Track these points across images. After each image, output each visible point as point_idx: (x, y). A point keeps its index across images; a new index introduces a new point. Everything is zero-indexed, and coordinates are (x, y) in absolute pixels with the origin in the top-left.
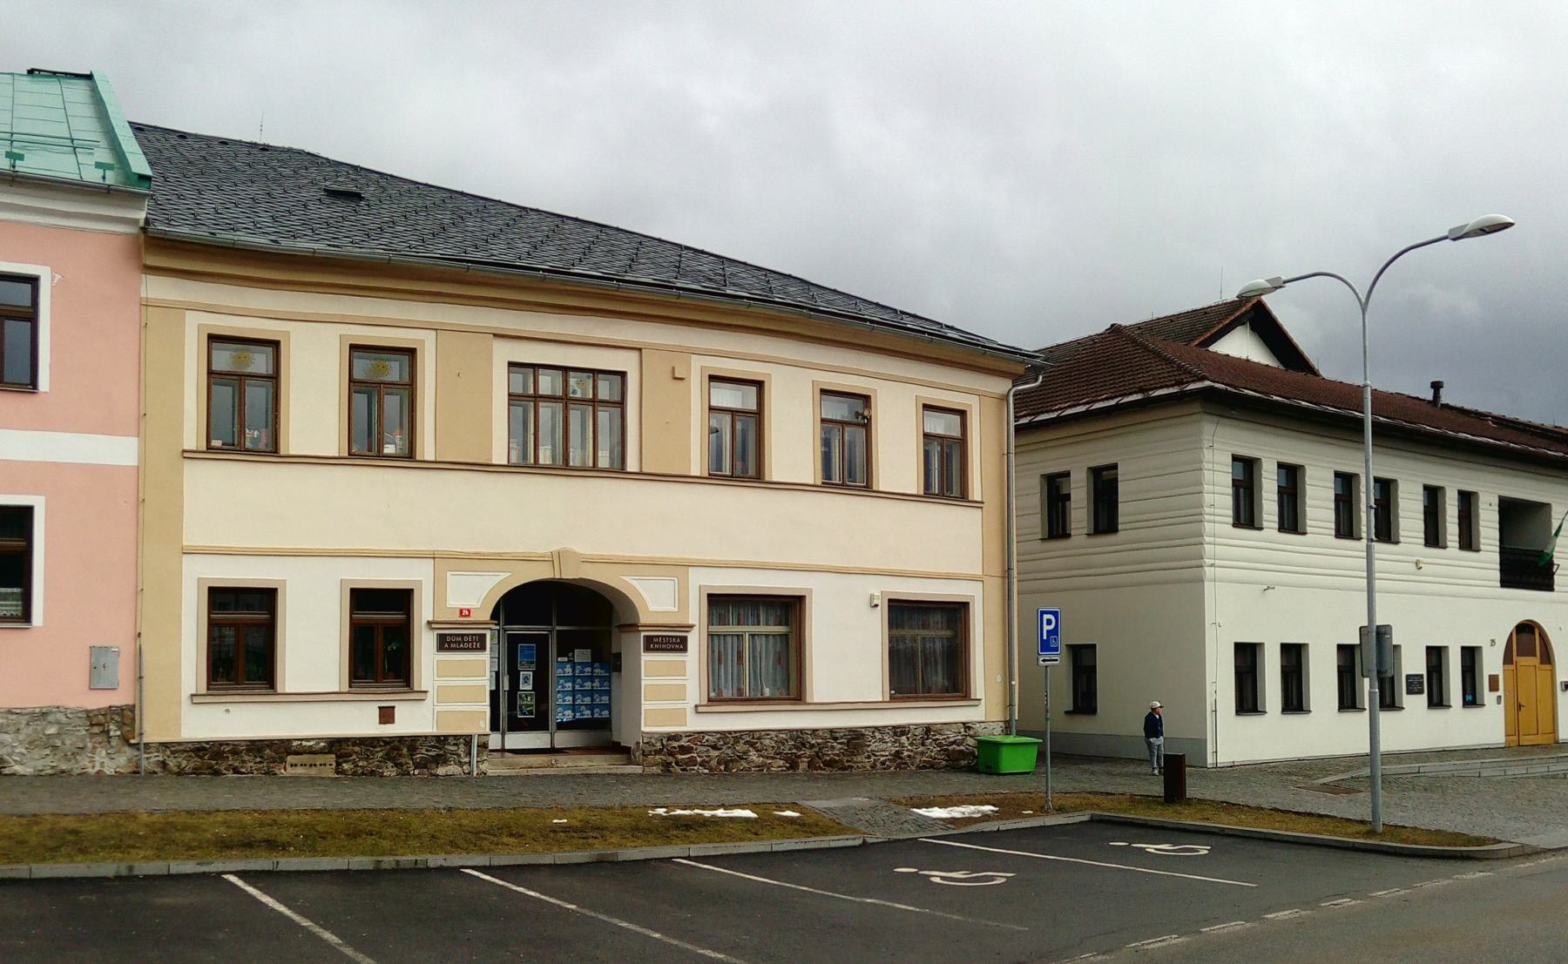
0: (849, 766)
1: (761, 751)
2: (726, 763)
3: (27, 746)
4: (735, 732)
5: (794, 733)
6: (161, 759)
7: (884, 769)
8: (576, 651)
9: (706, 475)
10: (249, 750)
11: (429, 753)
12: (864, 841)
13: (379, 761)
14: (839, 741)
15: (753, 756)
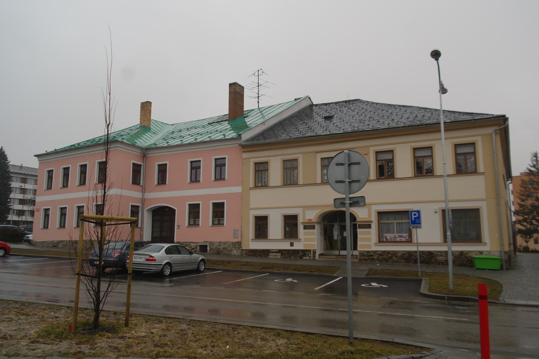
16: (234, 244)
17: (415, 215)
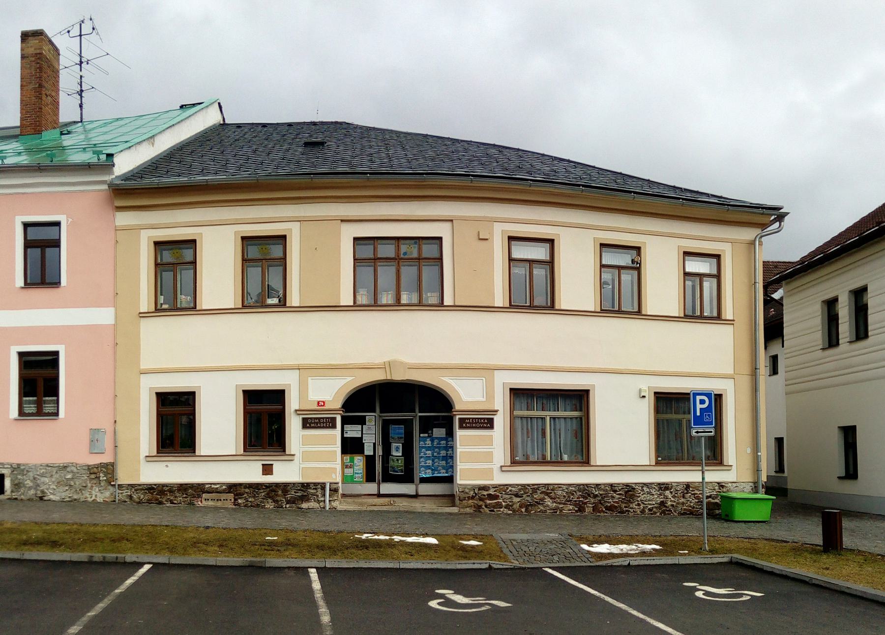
0: (627, 511)
1: (554, 499)
2: (527, 507)
3: (56, 485)
4: (533, 485)
5: (581, 486)
6: (129, 494)
7: (651, 514)
8: (434, 429)
9: (599, 310)
10: (179, 490)
11: (296, 494)
12: (490, 565)
13: (262, 498)
15: (548, 502)
16: (94, 471)
17: (702, 402)
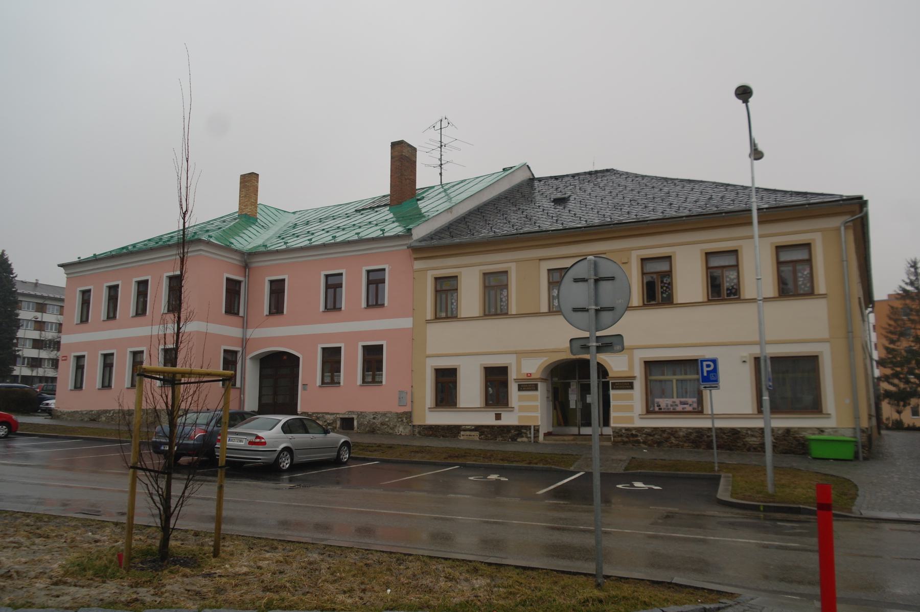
14: (727, 434)
16: (399, 416)
17: (708, 366)
